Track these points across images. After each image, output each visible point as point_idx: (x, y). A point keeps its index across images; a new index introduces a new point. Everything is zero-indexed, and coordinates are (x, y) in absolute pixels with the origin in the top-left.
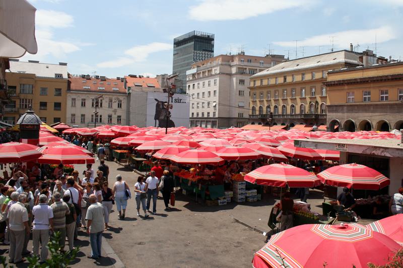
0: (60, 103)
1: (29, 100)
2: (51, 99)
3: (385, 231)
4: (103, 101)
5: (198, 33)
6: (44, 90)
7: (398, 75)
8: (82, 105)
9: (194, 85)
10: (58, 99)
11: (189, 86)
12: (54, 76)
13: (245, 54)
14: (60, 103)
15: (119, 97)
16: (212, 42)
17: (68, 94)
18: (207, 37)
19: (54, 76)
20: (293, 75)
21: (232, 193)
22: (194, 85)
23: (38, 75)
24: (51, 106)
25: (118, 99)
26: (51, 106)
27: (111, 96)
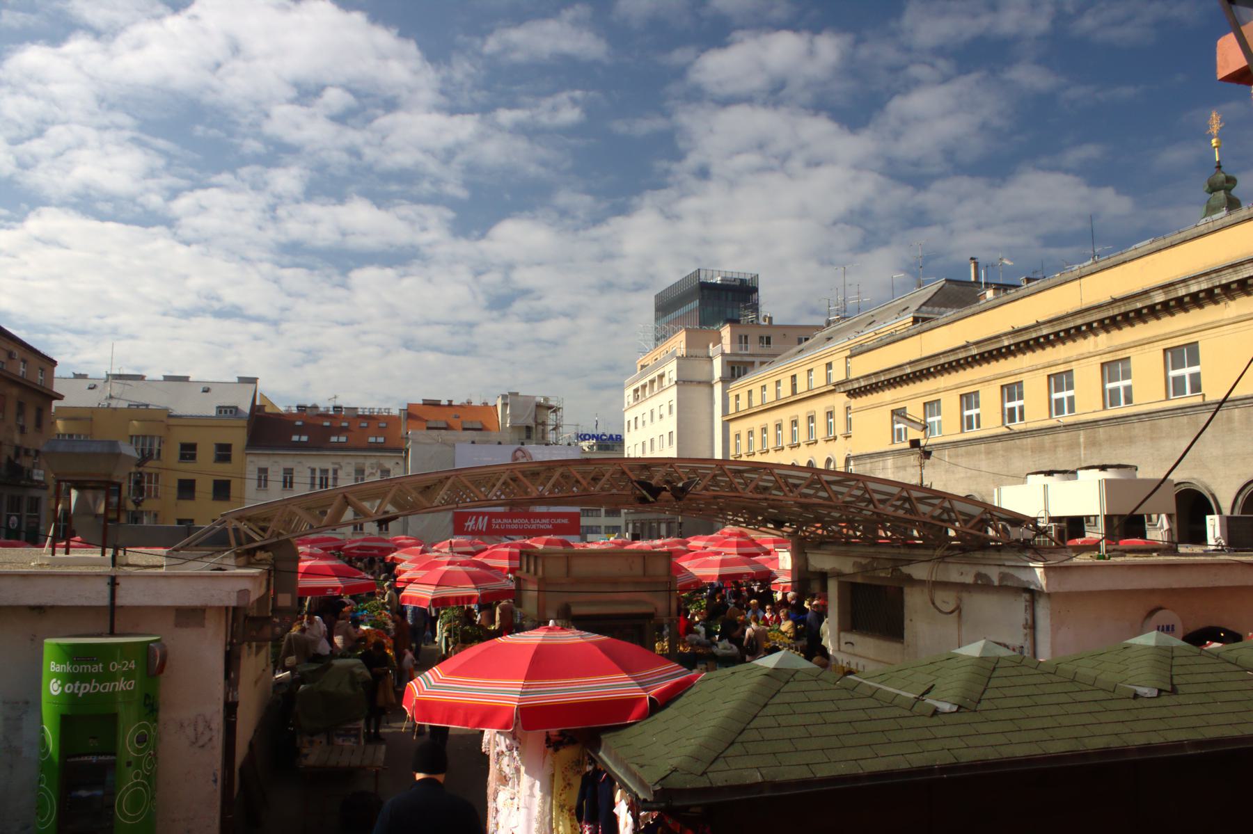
0: (216, 482)
1: (150, 475)
2: (205, 470)
3: (1047, 585)
4: (340, 472)
5: (710, 274)
6: (188, 452)
7: (944, 769)
8: (285, 486)
9: (750, 392)
10: (223, 471)
11: (737, 397)
12: (213, 413)
13: (775, 322)
14: (216, 482)
15: (382, 461)
16: (755, 296)
17: (249, 458)
18: (737, 283)
19: (213, 413)
20: (777, 400)
21: (488, 734)
22: (750, 392)
23: (178, 410)
24: (204, 487)
25: (380, 466)
26: (204, 487)
27: (361, 460)
